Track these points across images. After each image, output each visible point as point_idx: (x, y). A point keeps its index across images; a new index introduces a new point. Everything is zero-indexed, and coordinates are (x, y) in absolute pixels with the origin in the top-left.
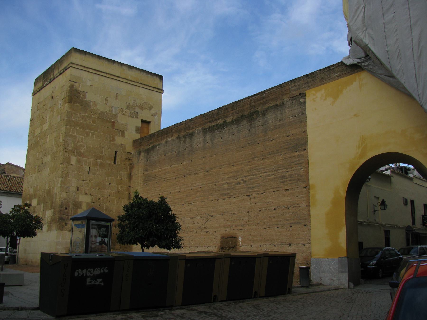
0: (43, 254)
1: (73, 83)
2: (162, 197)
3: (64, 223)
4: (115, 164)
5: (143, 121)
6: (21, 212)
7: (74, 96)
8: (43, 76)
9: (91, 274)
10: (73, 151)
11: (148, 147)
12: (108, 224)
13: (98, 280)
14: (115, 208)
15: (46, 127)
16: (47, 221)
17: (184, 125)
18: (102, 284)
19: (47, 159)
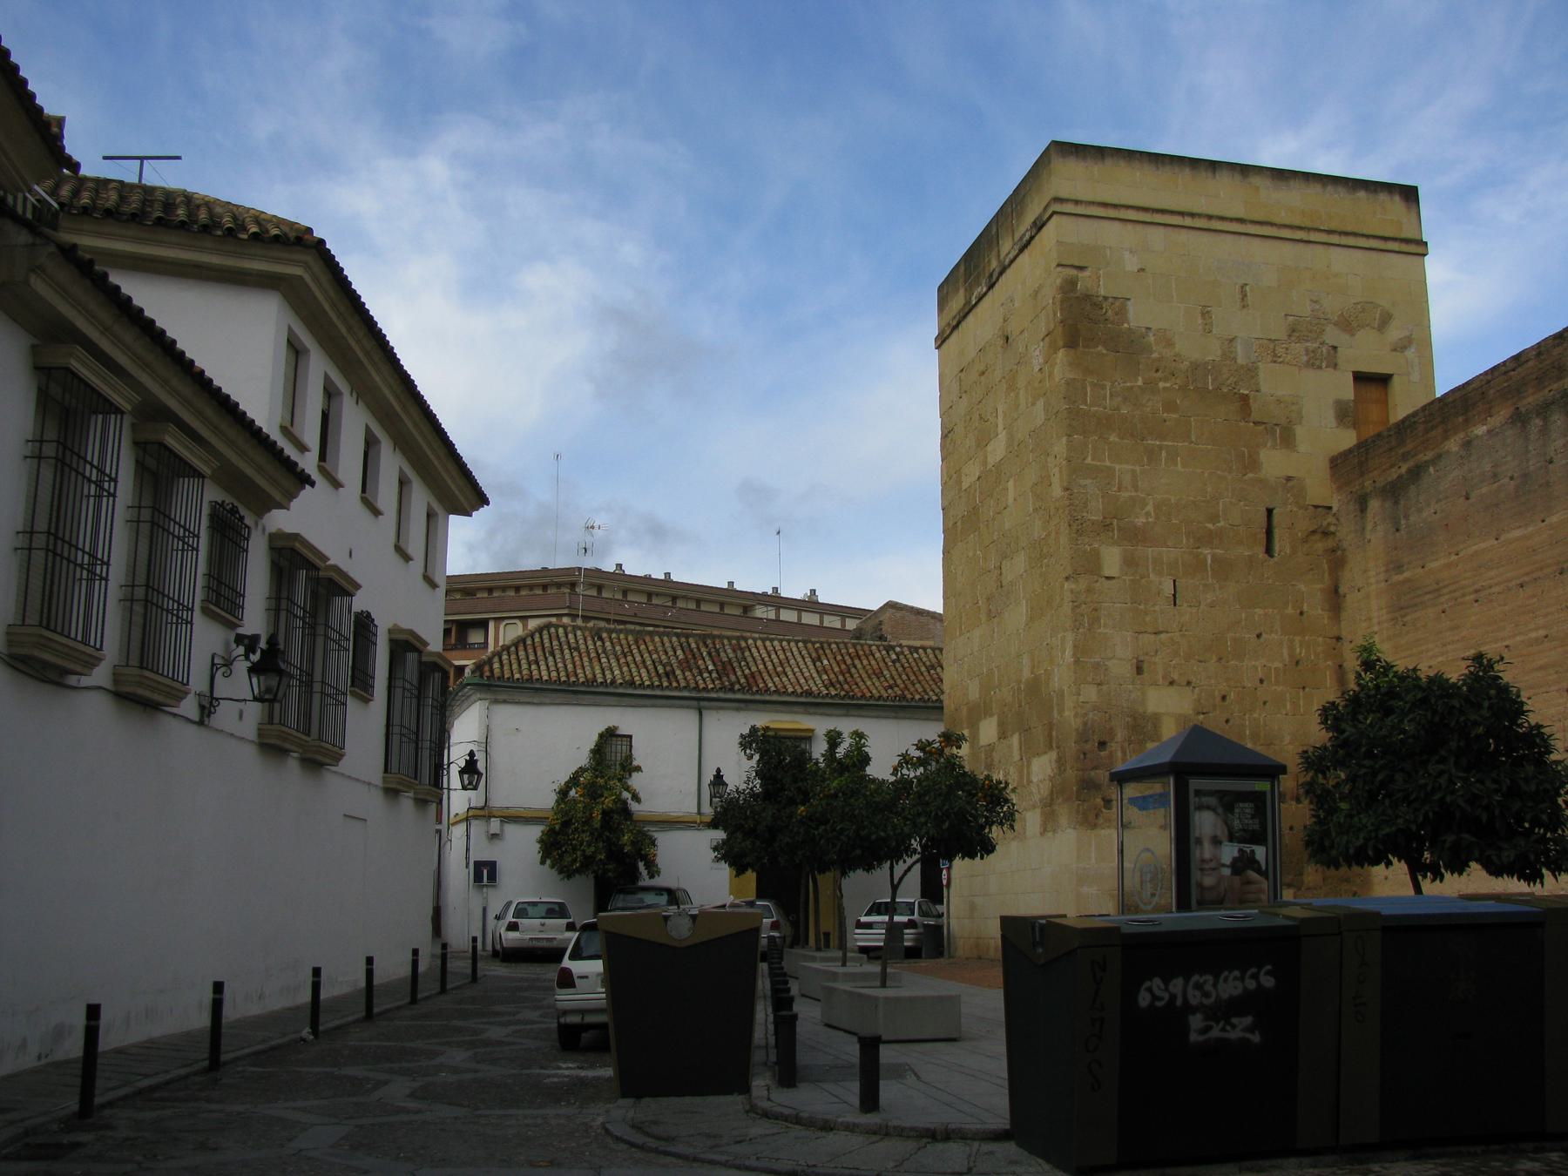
0: (1008, 923)
1: (1074, 272)
2: (1478, 658)
3: (1099, 801)
4: (1271, 556)
5: (1360, 378)
6: (933, 766)
7: (1084, 321)
8: (962, 268)
9: (1206, 995)
10: (1107, 527)
11: (1393, 475)
12: (1262, 786)
13: (1235, 1020)
14: (1289, 727)
15: (997, 449)
16: (1037, 797)
17: (1531, 363)
18: (1256, 1038)
19: (1018, 566)
